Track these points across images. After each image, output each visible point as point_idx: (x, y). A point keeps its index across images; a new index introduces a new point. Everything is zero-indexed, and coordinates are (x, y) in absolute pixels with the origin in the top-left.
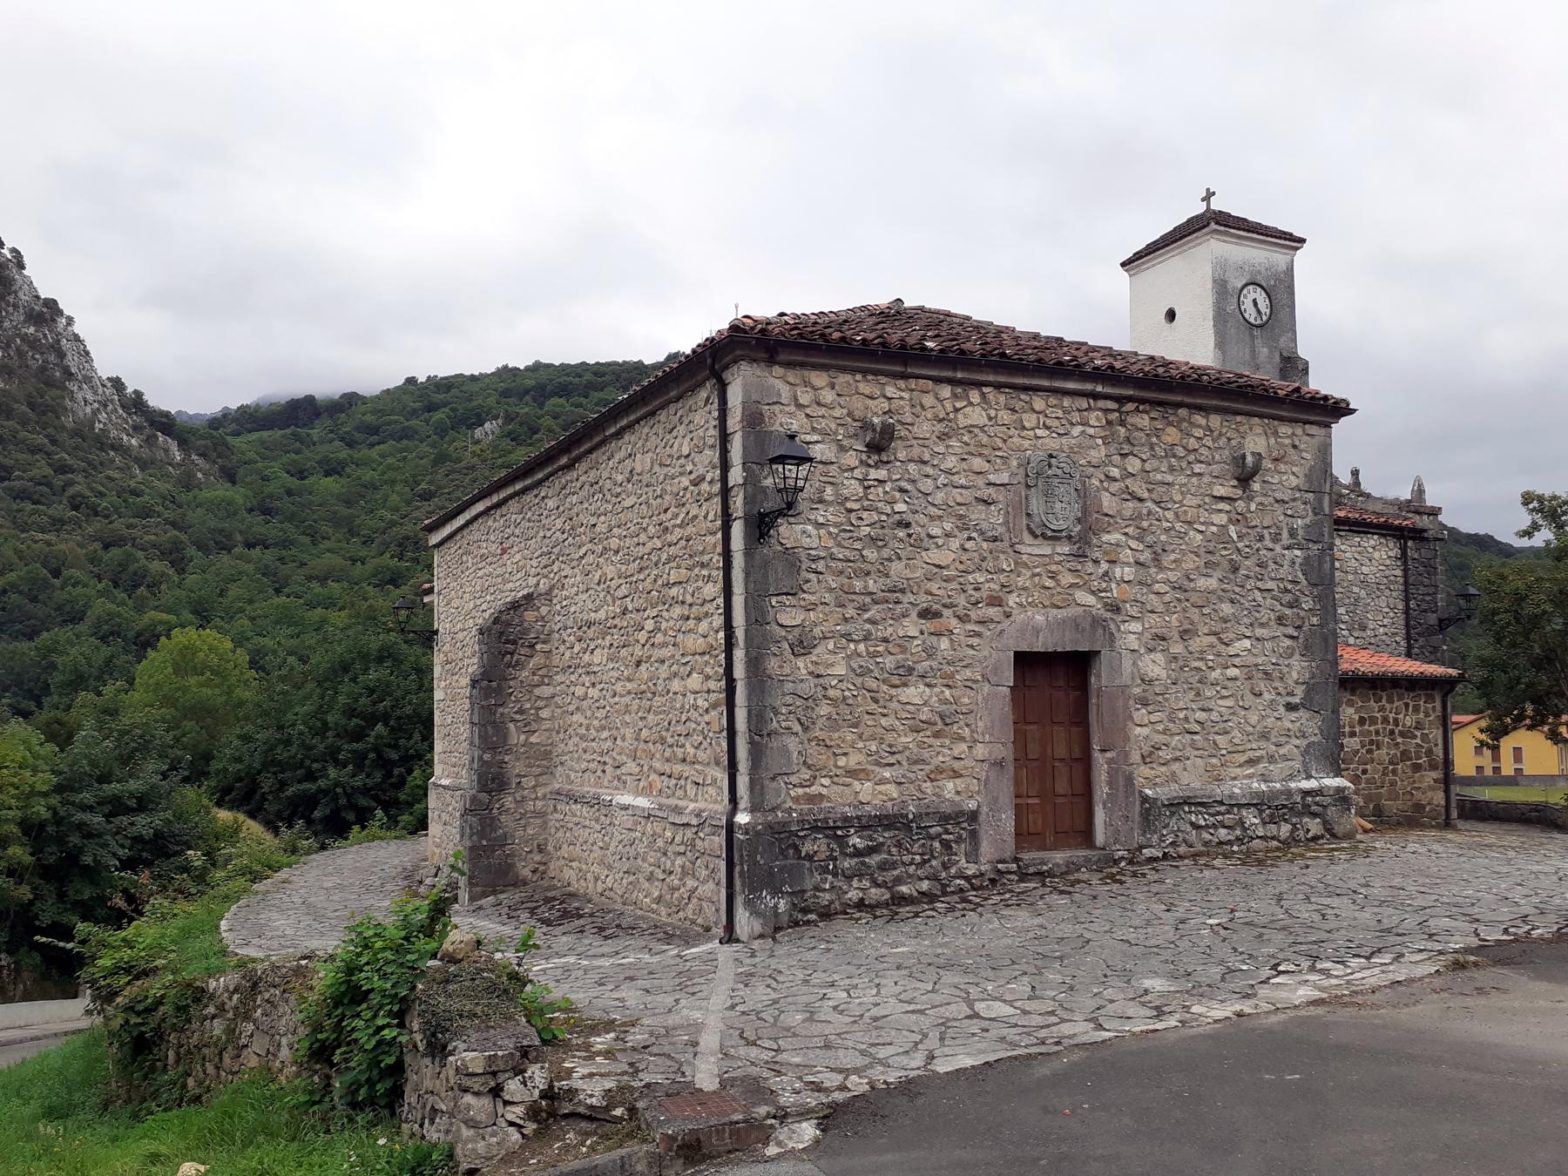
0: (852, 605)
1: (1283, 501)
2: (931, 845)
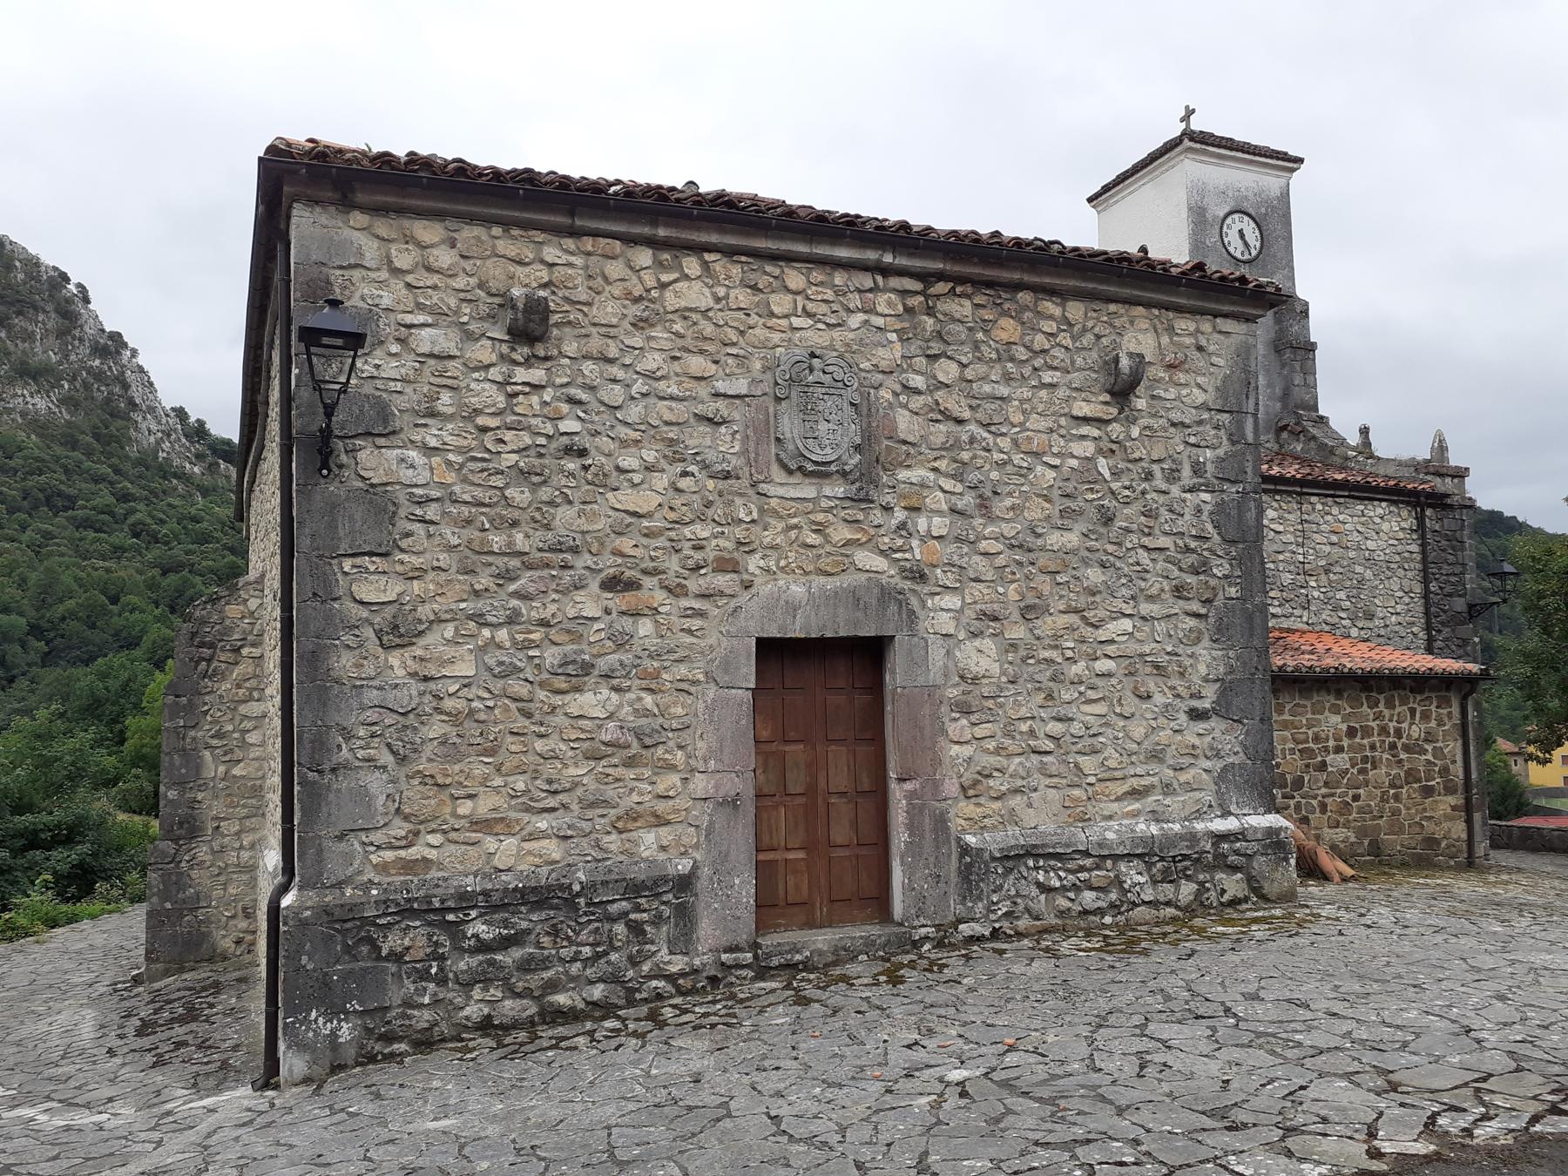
0: (488, 571)
1: (1182, 424)
2: (611, 930)
